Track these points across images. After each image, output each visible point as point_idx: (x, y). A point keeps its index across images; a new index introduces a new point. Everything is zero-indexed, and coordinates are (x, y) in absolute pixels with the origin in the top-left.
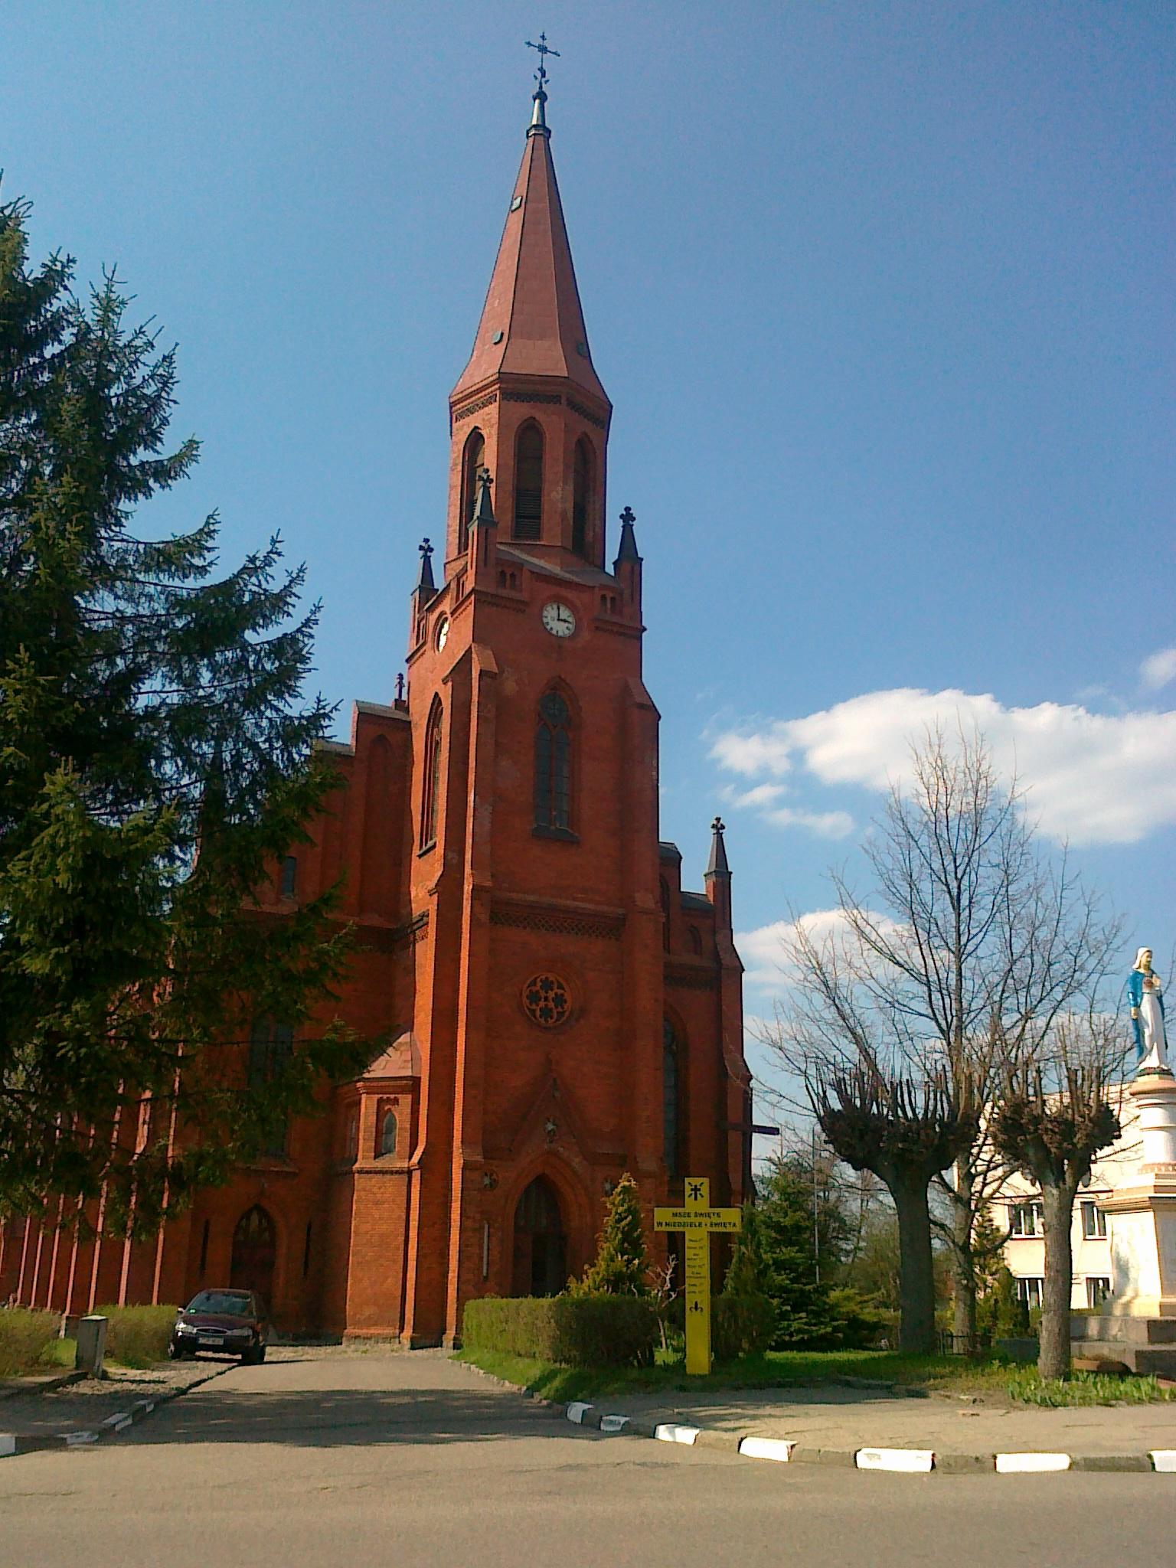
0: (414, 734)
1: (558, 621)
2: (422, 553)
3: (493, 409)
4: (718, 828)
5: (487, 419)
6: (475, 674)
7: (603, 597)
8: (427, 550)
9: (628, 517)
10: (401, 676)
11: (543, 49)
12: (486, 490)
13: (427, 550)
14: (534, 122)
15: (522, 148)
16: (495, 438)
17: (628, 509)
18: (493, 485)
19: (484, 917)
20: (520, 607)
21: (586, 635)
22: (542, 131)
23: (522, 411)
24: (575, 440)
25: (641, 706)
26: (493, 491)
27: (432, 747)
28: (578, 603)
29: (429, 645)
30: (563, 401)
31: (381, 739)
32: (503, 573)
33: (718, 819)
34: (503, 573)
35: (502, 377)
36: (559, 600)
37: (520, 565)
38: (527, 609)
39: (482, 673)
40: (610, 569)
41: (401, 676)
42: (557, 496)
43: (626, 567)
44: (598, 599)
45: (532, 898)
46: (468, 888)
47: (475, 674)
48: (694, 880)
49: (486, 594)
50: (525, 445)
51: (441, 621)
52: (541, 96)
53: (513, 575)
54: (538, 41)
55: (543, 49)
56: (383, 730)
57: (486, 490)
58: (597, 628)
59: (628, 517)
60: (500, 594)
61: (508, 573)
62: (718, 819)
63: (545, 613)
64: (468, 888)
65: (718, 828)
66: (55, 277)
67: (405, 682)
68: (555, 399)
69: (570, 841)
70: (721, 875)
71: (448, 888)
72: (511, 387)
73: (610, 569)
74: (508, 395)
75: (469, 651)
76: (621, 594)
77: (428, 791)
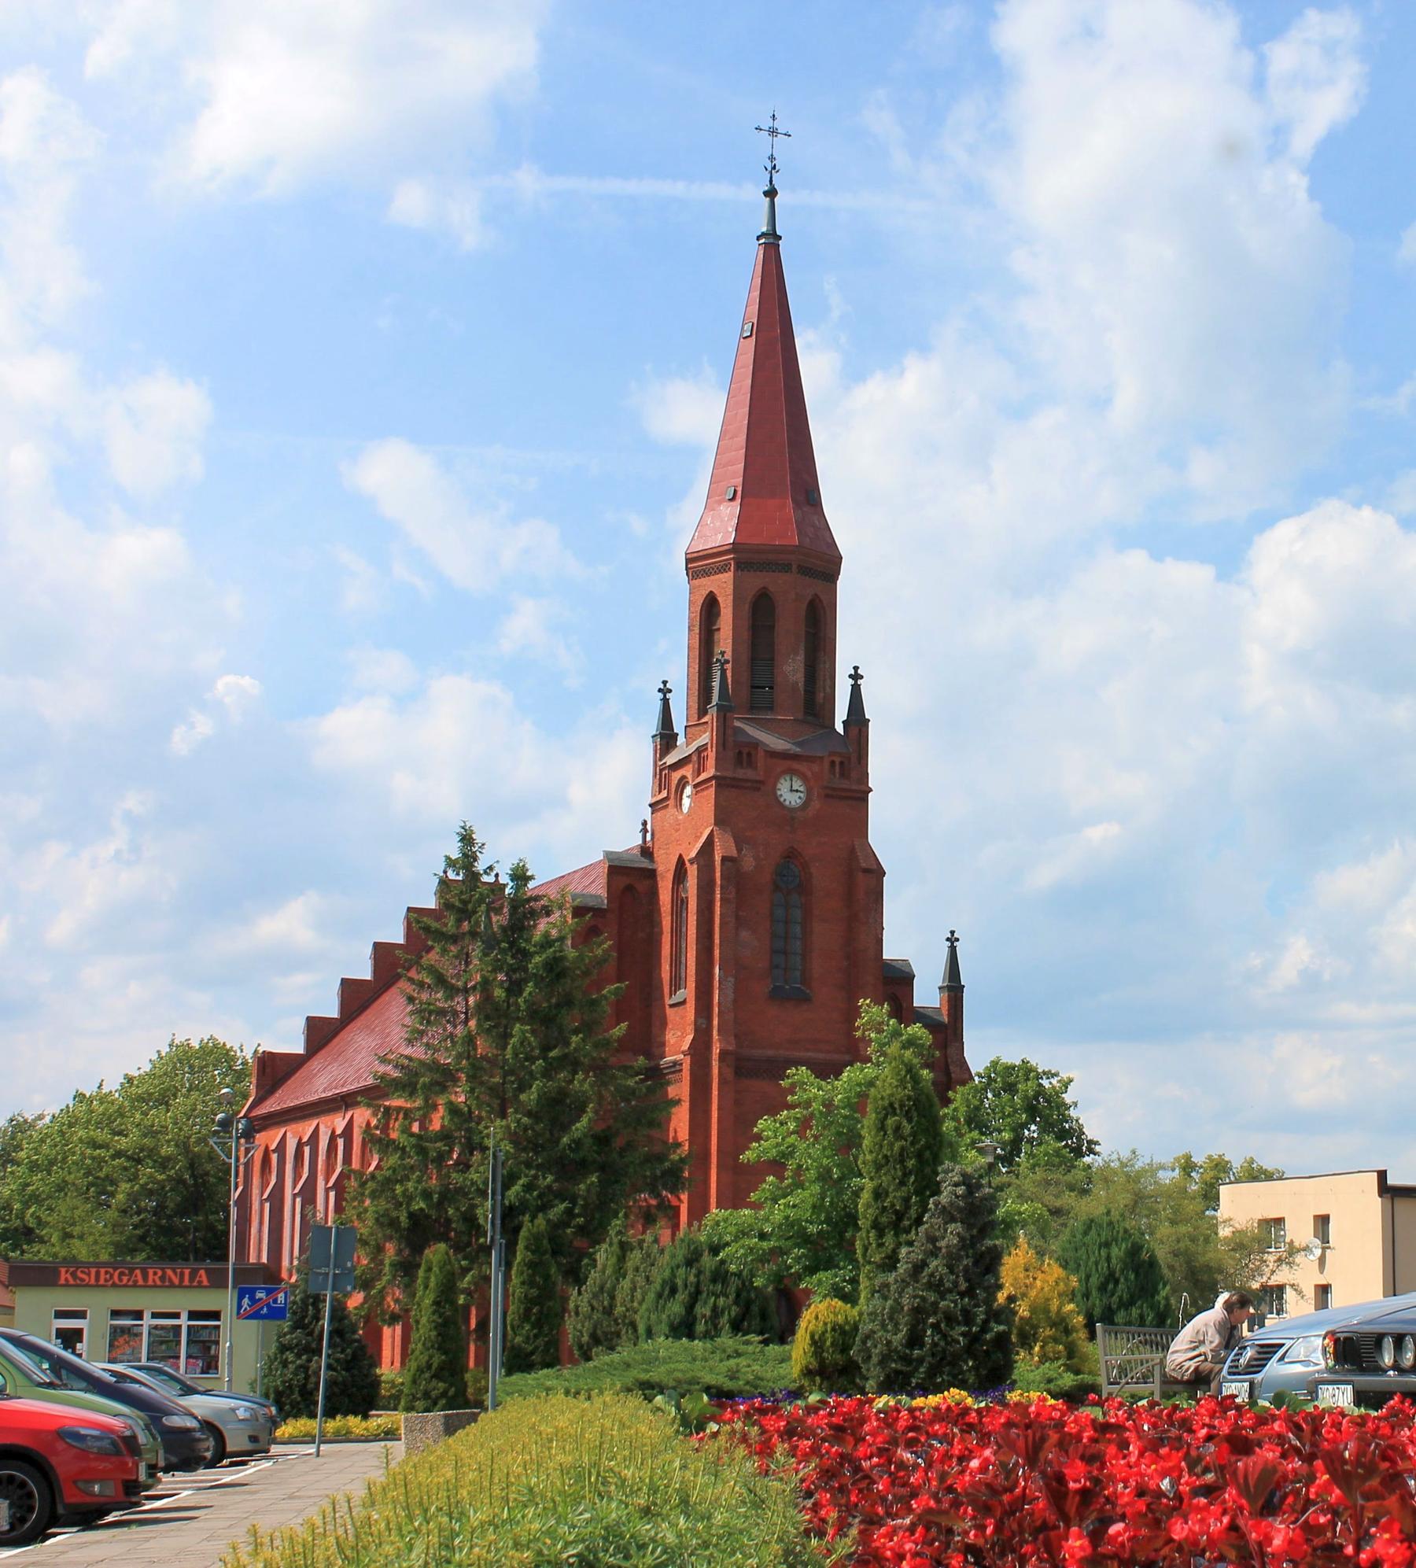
0: (660, 884)
1: (790, 793)
2: (661, 695)
3: (728, 577)
4: (952, 940)
5: (723, 584)
6: (718, 858)
7: (833, 763)
8: (665, 691)
9: (856, 676)
10: (645, 823)
11: (773, 132)
12: (723, 672)
13: (665, 691)
14: (764, 229)
15: (752, 254)
16: (730, 604)
17: (856, 668)
18: (729, 666)
19: (729, 1074)
20: (757, 786)
21: (816, 804)
22: (771, 241)
23: (757, 581)
24: (804, 606)
25: (866, 871)
26: (729, 674)
27: (679, 904)
28: (809, 774)
29: (671, 802)
30: (794, 567)
31: (629, 888)
32: (740, 753)
33: (952, 933)
34: (740, 753)
35: (735, 547)
36: (792, 772)
37: (756, 744)
38: (764, 787)
39: (724, 859)
40: (839, 728)
41: (645, 823)
42: (792, 669)
43: (854, 731)
44: (826, 765)
45: (770, 1053)
46: (716, 1051)
47: (718, 858)
48: (927, 994)
49: (724, 778)
50: (759, 614)
51: (682, 783)
52: (771, 193)
53: (749, 754)
54: (767, 124)
55: (773, 132)
56: (630, 878)
57: (723, 672)
58: (827, 796)
59: (856, 676)
60: (739, 776)
61: (745, 751)
62: (952, 933)
63: (779, 786)
64: (716, 1051)
65: (952, 940)
66: (520, 876)
67: (649, 827)
68: (786, 568)
69: (802, 998)
70: (954, 988)
71: (699, 1050)
72: (744, 556)
73: (839, 728)
74: (741, 566)
75: (711, 836)
76: (849, 759)
77: (679, 951)
